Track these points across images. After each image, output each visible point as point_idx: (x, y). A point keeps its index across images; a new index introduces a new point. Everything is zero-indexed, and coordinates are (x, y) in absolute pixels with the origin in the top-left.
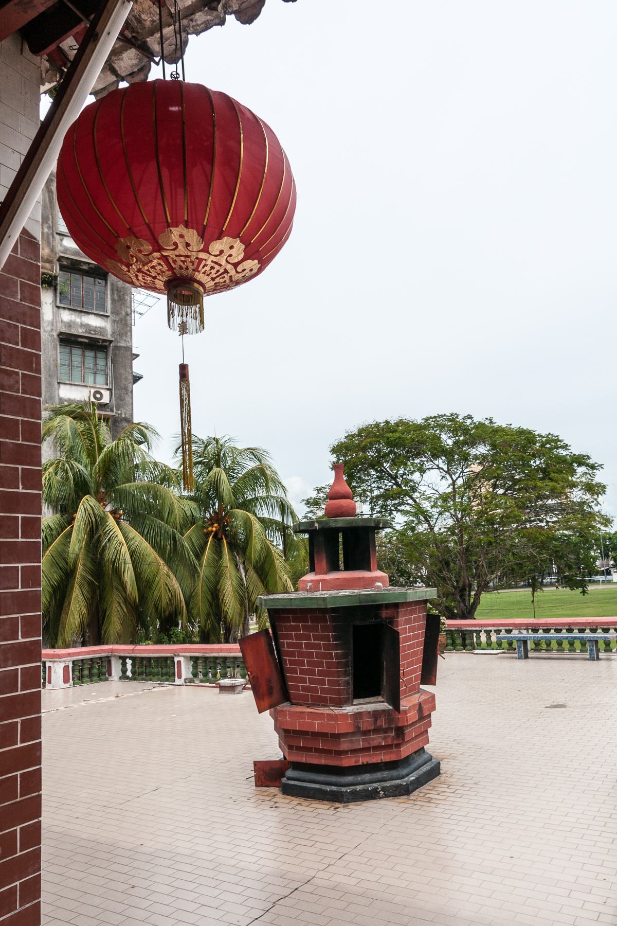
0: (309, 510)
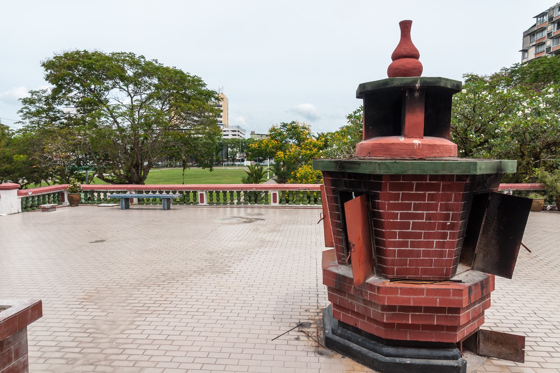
0: (24, 106)
